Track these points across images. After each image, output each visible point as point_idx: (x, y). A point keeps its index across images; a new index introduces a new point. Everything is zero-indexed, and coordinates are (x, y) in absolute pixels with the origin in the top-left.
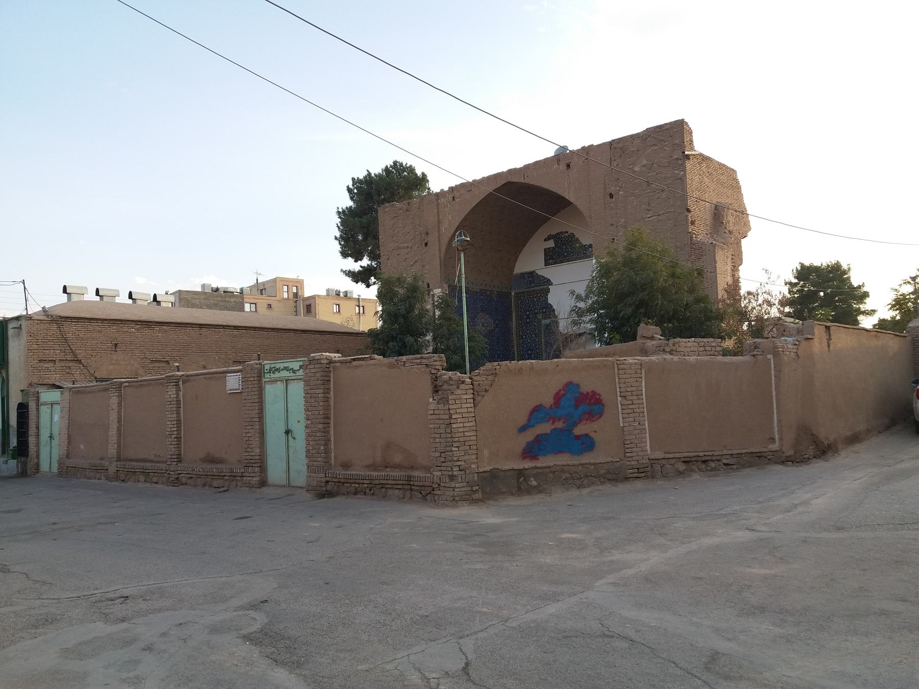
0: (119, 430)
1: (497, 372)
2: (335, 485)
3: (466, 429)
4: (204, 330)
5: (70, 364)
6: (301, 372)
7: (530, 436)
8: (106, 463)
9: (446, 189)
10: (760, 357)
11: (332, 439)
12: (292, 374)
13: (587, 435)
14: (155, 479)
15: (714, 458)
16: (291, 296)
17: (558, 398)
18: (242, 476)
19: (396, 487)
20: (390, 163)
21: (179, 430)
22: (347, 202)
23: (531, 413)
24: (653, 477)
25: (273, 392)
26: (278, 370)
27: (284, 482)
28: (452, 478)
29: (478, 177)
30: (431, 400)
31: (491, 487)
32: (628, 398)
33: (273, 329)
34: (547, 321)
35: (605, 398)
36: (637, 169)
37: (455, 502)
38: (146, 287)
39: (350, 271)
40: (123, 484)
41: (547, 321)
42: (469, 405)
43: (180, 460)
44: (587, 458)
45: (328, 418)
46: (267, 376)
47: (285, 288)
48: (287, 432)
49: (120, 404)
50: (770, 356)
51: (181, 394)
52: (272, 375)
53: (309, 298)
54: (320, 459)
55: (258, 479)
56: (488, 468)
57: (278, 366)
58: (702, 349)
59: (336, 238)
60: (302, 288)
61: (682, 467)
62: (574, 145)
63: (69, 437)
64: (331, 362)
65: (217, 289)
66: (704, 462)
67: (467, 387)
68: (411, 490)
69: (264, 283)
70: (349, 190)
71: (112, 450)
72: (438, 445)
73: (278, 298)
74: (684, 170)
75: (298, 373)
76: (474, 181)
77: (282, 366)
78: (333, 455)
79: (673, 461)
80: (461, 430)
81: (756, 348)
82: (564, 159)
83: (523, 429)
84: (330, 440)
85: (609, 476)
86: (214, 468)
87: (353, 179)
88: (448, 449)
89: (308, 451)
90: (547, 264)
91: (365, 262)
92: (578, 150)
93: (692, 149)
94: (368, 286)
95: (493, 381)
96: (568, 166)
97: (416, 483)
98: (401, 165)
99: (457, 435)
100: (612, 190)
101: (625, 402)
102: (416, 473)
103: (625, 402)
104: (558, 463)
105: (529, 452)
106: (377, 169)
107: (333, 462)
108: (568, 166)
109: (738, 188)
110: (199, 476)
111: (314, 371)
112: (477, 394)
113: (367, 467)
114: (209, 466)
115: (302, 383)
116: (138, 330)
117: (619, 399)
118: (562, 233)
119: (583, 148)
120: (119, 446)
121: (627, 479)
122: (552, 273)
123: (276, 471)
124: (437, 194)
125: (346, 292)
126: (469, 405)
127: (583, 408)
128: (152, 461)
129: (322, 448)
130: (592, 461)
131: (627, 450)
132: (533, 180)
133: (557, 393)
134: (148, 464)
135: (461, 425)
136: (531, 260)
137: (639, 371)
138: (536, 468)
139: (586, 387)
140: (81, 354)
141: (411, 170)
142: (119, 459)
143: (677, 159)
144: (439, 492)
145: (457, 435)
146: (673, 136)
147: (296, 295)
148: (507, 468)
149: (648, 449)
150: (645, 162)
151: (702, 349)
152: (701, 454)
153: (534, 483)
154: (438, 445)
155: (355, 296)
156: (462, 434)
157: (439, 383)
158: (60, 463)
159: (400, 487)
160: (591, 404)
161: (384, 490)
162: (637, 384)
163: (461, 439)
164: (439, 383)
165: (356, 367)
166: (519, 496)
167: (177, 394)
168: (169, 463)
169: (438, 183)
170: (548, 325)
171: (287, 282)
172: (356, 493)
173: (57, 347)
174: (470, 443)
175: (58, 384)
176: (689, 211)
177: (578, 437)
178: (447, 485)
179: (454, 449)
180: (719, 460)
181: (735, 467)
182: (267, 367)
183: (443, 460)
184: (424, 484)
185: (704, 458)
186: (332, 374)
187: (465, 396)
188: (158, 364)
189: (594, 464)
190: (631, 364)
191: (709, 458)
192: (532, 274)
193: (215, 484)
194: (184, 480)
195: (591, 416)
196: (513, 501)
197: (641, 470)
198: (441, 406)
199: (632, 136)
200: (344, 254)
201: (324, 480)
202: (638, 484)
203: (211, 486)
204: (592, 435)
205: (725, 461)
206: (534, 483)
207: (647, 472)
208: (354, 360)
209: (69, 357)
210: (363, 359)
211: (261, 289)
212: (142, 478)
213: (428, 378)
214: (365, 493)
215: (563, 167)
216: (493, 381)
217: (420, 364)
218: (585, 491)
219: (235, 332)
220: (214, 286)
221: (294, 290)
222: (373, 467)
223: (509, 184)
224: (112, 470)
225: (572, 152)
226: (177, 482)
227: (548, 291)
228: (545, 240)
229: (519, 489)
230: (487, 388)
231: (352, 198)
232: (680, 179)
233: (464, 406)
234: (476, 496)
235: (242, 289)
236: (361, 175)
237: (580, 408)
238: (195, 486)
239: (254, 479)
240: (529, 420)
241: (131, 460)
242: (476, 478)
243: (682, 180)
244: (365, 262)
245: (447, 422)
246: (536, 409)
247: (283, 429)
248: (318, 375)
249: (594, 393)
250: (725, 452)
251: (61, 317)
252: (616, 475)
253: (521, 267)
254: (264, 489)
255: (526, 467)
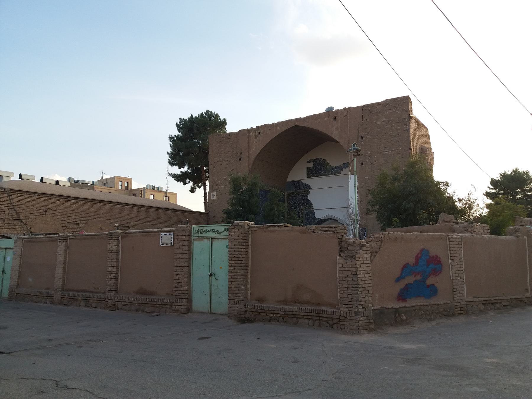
0: (64, 269)
1: (383, 239)
2: (250, 313)
3: (366, 279)
4: (102, 204)
5: (15, 222)
6: (226, 233)
7: (402, 285)
8: (52, 292)
9: (255, 127)
10: (520, 237)
11: (249, 281)
12: (217, 235)
13: (433, 285)
14: (94, 305)
15: (499, 301)
16: (124, 188)
17: (417, 258)
18: (172, 305)
19: (306, 317)
20: (204, 111)
21: (117, 271)
22: (175, 132)
23: (403, 269)
24: (467, 314)
25: (200, 248)
26: (205, 231)
27: (207, 310)
28: (357, 313)
29: (276, 121)
30: (338, 257)
31: (383, 319)
32: (455, 261)
33: (144, 206)
34: (308, 211)
35: (443, 260)
36: (379, 123)
37: (358, 331)
38: (52, 177)
39: (174, 174)
40: (66, 307)
41: (308, 211)
42: (368, 262)
43: (116, 292)
44: (434, 301)
45: (247, 266)
46: (196, 235)
47: (120, 183)
48: (211, 275)
49: (66, 251)
50: (525, 237)
51: (120, 245)
52: (200, 235)
53: (135, 190)
54: (240, 295)
55: (186, 307)
56: (378, 307)
57: (205, 229)
58: (482, 231)
59: (168, 153)
60: (131, 184)
61: (482, 307)
62: (338, 106)
63: (20, 272)
64: (250, 227)
65: (78, 181)
66: (493, 304)
67: (367, 249)
68: (320, 319)
69: (106, 179)
70: (177, 125)
71: (58, 283)
72: (345, 289)
73: (115, 189)
74: (409, 125)
75: (222, 234)
76: (273, 124)
77: (209, 229)
78: (249, 292)
79: (477, 303)
80: (363, 279)
81: (516, 231)
82: (330, 114)
83: (398, 280)
84: (247, 282)
85: (445, 313)
86: (147, 299)
87: (180, 119)
88: (354, 292)
89: (230, 289)
90: (308, 176)
91: (186, 169)
92: (341, 110)
93: (412, 114)
94: (185, 184)
95: (381, 245)
96: (335, 118)
97: (325, 316)
98: (211, 113)
99: (361, 283)
100: (363, 134)
101: (453, 263)
102: (324, 308)
103: (453, 263)
104: (418, 304)
105: (402, 296)
106: (196, 114)
107: (249, 297)
108: (335, 118)
109: (429, 139)
110: (133, 304)
111: (238, 233)
112: (374, 253)
113: (280, 302)
114: (143, 297)
115: (227, 241)
116: (61, 201)
117: (450, 261)
118: (318, 159)
119: (345, 109)
120: (64, 280)
121: (454, 315)
122: (313, 182)
123: (200, 301)
124: (230, 134)
125: (158, 188)
126: (368, 262)
127: (431, 266)
128: (91, 292)
129: (242, 287)
130: (436, 303)
131: (455, 296)
132: (310, 126)
133: (417, 256)
134: (88, 294)
135: (363, 276)
136: (298, 174)
137: (460, 243)
138: (406, 307)
139: (433, 253)
140: (22, 216)
141: (217, 116)
142: (63, 290)
143: (405, 119)
144: (345, 323)
145: (361, 283)
146: (402, 105)
147: (127, 188)
148: (390, 307)
149: (465, 295)
150: (384, 119)
151: (482, 231)
152: (492, 299)
153: (404, 318)
154: (345, 289)
155: (164, 190)
156: (363, 282)
157: (344, 244)
158: (11, 291)
159: (310, 317)
160: (434, 264)
161: (295, 319)
162: (459, 251)
163: (363, 286)
164: (344, 244)
165: (272, 231)
166: (396, 326)
167: (118, 246)
168: (107, 293)
169: (231, 128)
170: (307, 213)
171: (121, 179)
172: (270, 321)
173: (6, 210)
174: (369, 289)
175: (6, 235)
176: (410, 149)
177: (428, 286)
178: (352, 318)
179: (359, 293)
180: (500, 303)
181: (509, 307)
182: (196, 229)
183: (350, 300)
184: (332, 316)
185: (493, 301)
186: (250, 236)
187: (366, 256)
188: (72, 225)
189: (438, 305)
190: (456, 238)
191: (496, 301)
192: (298, 182)
193: (147, 309)
194: (120, 306)
195: (436, 272)
196: (392, 330)
197: (462, 309)
198: (349, 262)
199: (376, 103)
200: (171, 163)
201: (244, 310)
202: (462, 319)
203: (143, 311)
204: (436, 285)
205: (504, 304)
206: (404, 318)
207: (464, 311)
208: (269, 226)
209: (15, 217)
210: (278, 226)
211: (104, 183)
212: (83, 304)
213: (336, 241)
214: (278, 321)
215: (331, 119)
216: (381, 245)
217: (328, 231)
218: (434, 323)
219: (121, 207)
220: (76, 179)
221: (126, 184)
222: (285, 302)
223: (296, 127)
224: (57, 296)
225: (337, 111)
226: (114, 307)
227: (309, 192)
228: (308, 162)
229: (396, 321)
230: (377, 250)
231: (179, 130)
232: (406, 130)
233: (365, 262)
234: (372, 326)
235: (93, 182)
236: (186, 117)
237: (430, 266)
238: (129, 311)
239: (182, 307)
240: (401, 274)
241: (73, 291)
242: (372, 314)
243: (408, 131)
244: (186, 169)
245: (353, 273)
246: (405, 266)
247: (207, 273)
248: (241, 236)
249: (436, 256)
250: (505, 298)
251: (11, 190)
252: (449, 312)
253: (292, 177)
254: (190, 315)
255: (401, 306)
